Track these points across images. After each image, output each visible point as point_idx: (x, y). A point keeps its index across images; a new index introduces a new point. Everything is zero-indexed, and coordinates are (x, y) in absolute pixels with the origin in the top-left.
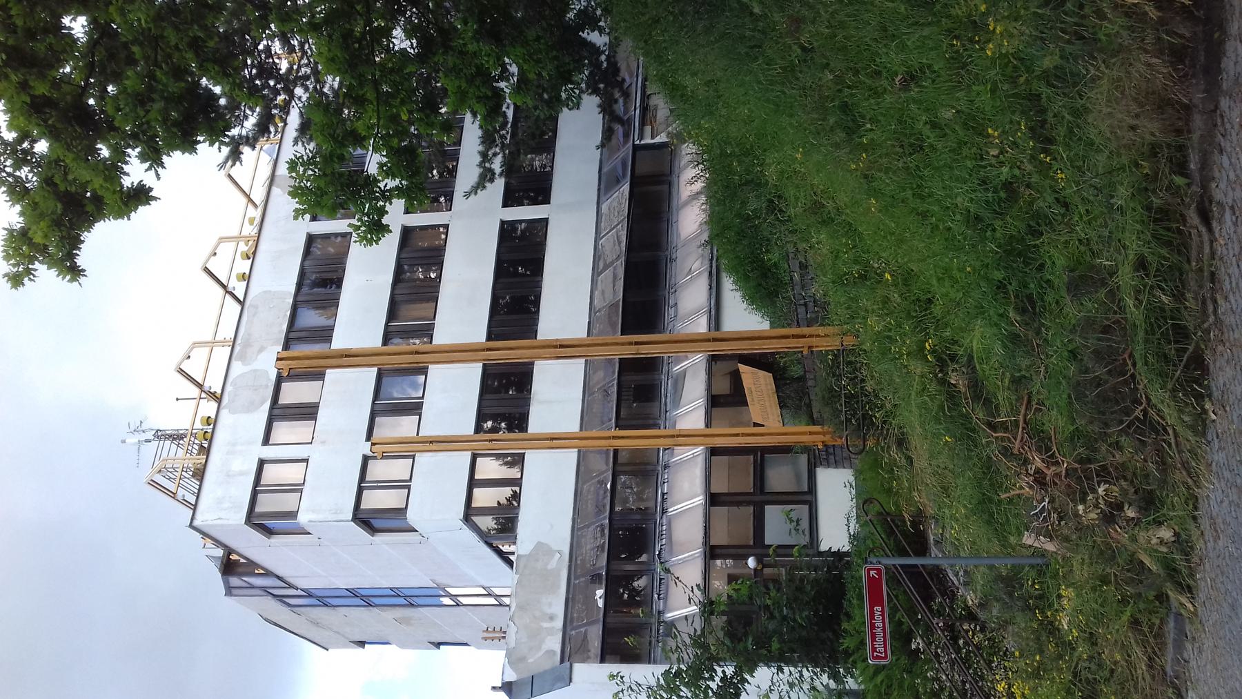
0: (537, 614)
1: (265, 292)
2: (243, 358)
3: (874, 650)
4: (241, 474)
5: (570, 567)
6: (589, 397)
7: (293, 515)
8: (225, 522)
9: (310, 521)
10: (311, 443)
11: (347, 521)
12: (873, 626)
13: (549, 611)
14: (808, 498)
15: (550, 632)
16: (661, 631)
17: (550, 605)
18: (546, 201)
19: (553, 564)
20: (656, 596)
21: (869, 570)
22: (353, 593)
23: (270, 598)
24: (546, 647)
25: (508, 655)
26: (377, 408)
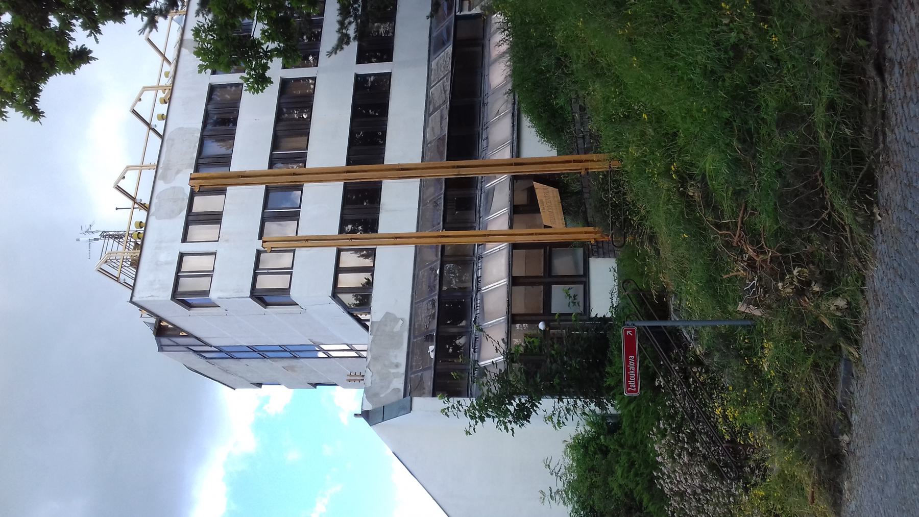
0: (386, 363)
1: (180, 129)
2: (164, 178)
3: (628, 386)
4: (167, 263)
6: (423, 206)
7: (206, 293)
8: (156, 298)
9: (218, 298)
11: (247, 297)
12: (628, 370)
13: (395, 361)
14: (583, 279)
15: (396, 375)
17: (396, 356)
18: (389, 58)
19: (397, 328)
20: (472, 350)
22: (253, 349)
24: (392, 386)
25: (366, 392)
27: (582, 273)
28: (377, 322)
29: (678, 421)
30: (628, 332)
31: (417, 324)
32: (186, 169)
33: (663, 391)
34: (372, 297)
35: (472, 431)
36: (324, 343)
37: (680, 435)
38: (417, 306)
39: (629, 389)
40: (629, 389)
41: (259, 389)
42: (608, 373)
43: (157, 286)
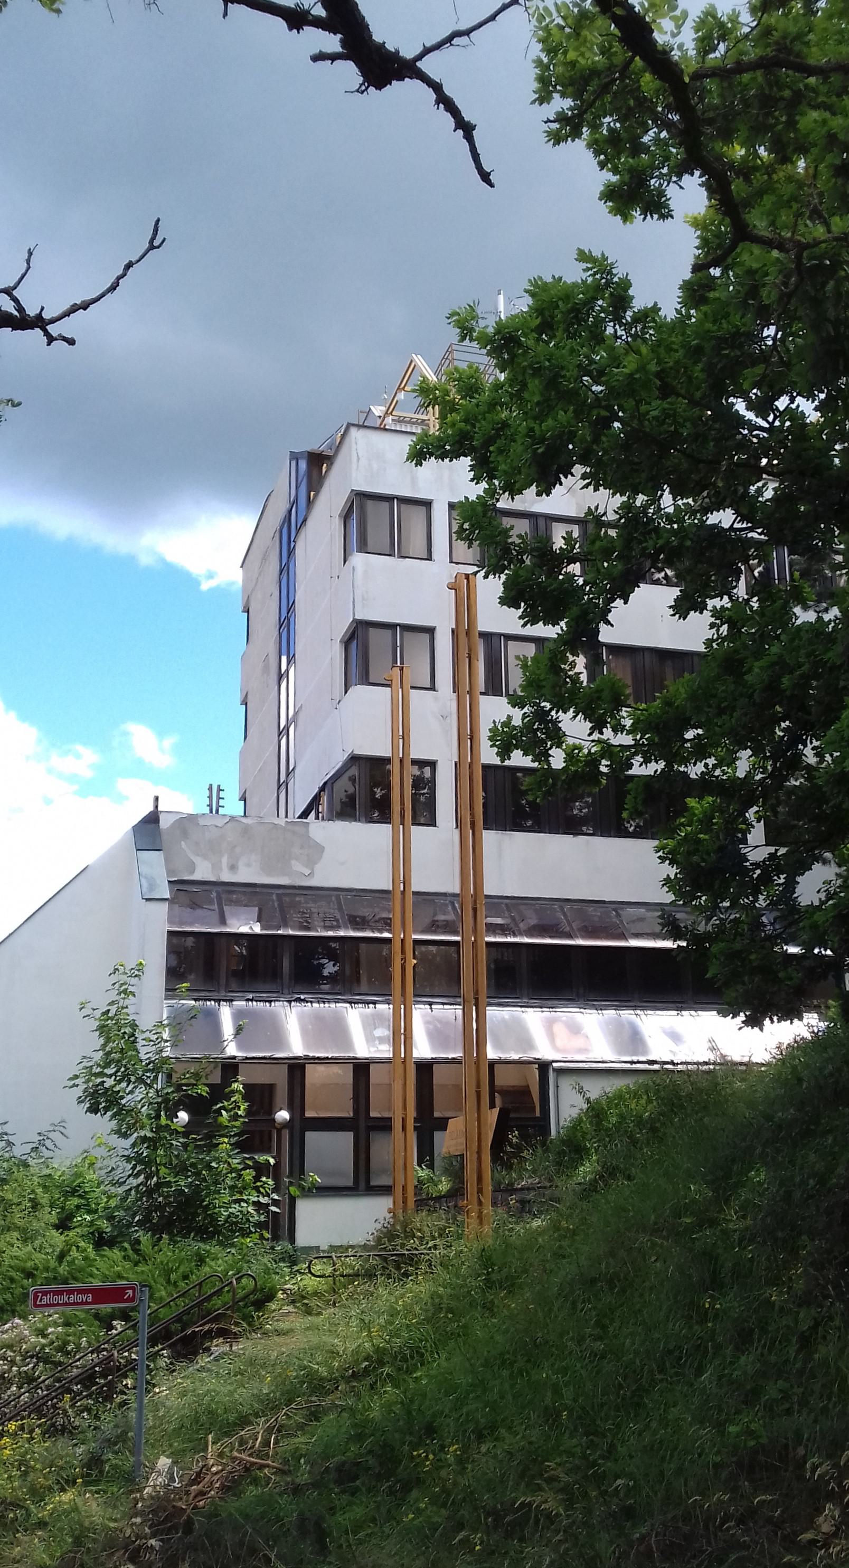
0: (238, 850)
3: (45, 1293)
5: (294, 887)
6: (506, 905)
7: (363, 547)
8: (354, 466)
10: (451, 562)
12: (70, 1292)
13: (241, 864)
14: (362, 1185)
15: (216, 867)
16: (208, 1003)
17: (248, 865)
20: (250, 996)
21: (133, 1289)
22: (291, 607)
23: (288, 506)
24: (198, 860)
25: (192, 818)
26: (495, 639)
27: (373, 1183)
28: (308, 831)
29: (55, 1356)
30: (130, 1292)
31: (302, 899)
32: (577, 504)
33: (102, 1333)
34: (350, 822)
35: (85, 1012)
36: (298, 728)
37: (35, 1360)
38: (333, 899)
39: (40, 1294)
40: (40, 1294)
41: (241, 609)
42: (160, 1239)
43: (375, 466)
